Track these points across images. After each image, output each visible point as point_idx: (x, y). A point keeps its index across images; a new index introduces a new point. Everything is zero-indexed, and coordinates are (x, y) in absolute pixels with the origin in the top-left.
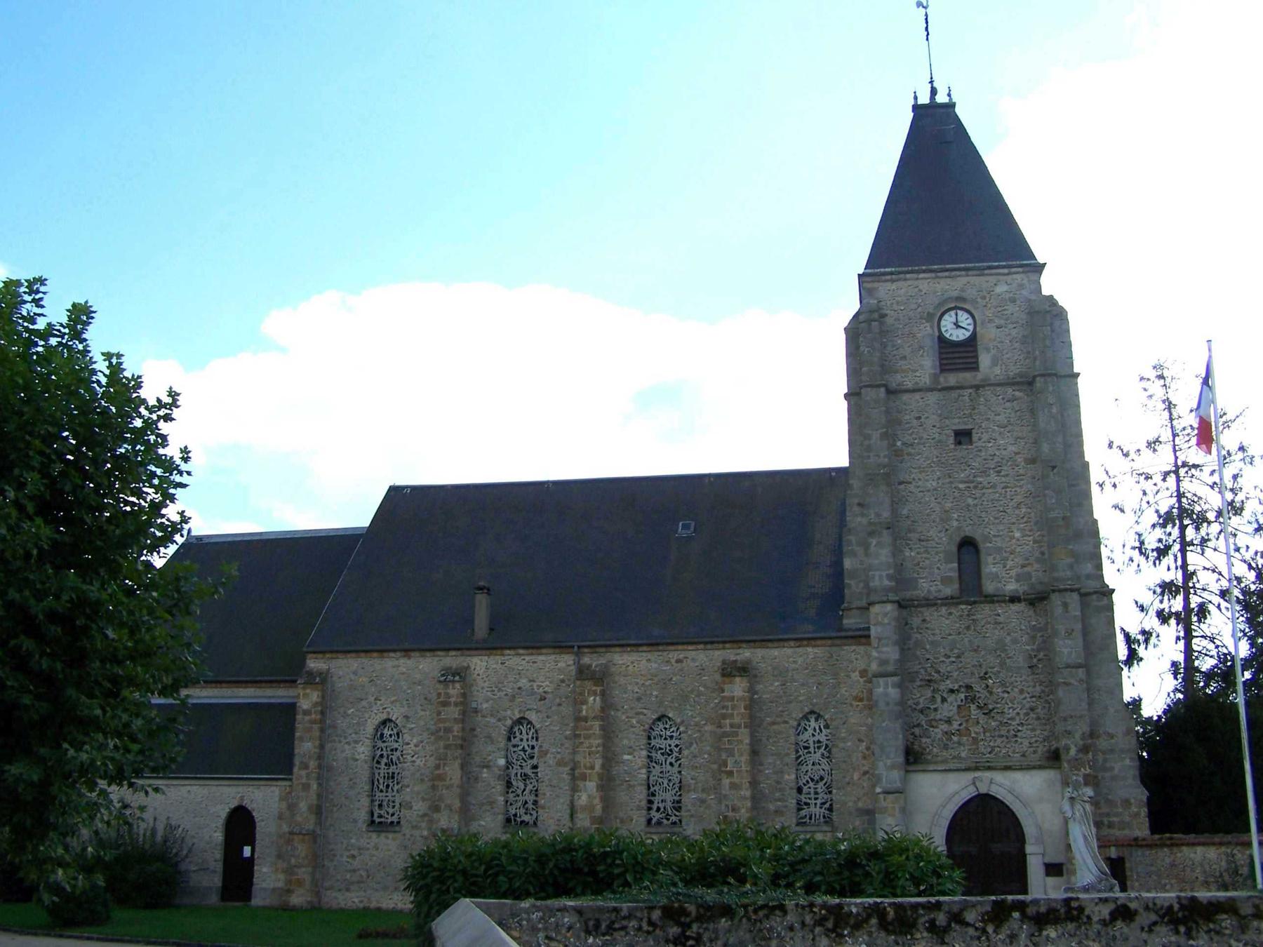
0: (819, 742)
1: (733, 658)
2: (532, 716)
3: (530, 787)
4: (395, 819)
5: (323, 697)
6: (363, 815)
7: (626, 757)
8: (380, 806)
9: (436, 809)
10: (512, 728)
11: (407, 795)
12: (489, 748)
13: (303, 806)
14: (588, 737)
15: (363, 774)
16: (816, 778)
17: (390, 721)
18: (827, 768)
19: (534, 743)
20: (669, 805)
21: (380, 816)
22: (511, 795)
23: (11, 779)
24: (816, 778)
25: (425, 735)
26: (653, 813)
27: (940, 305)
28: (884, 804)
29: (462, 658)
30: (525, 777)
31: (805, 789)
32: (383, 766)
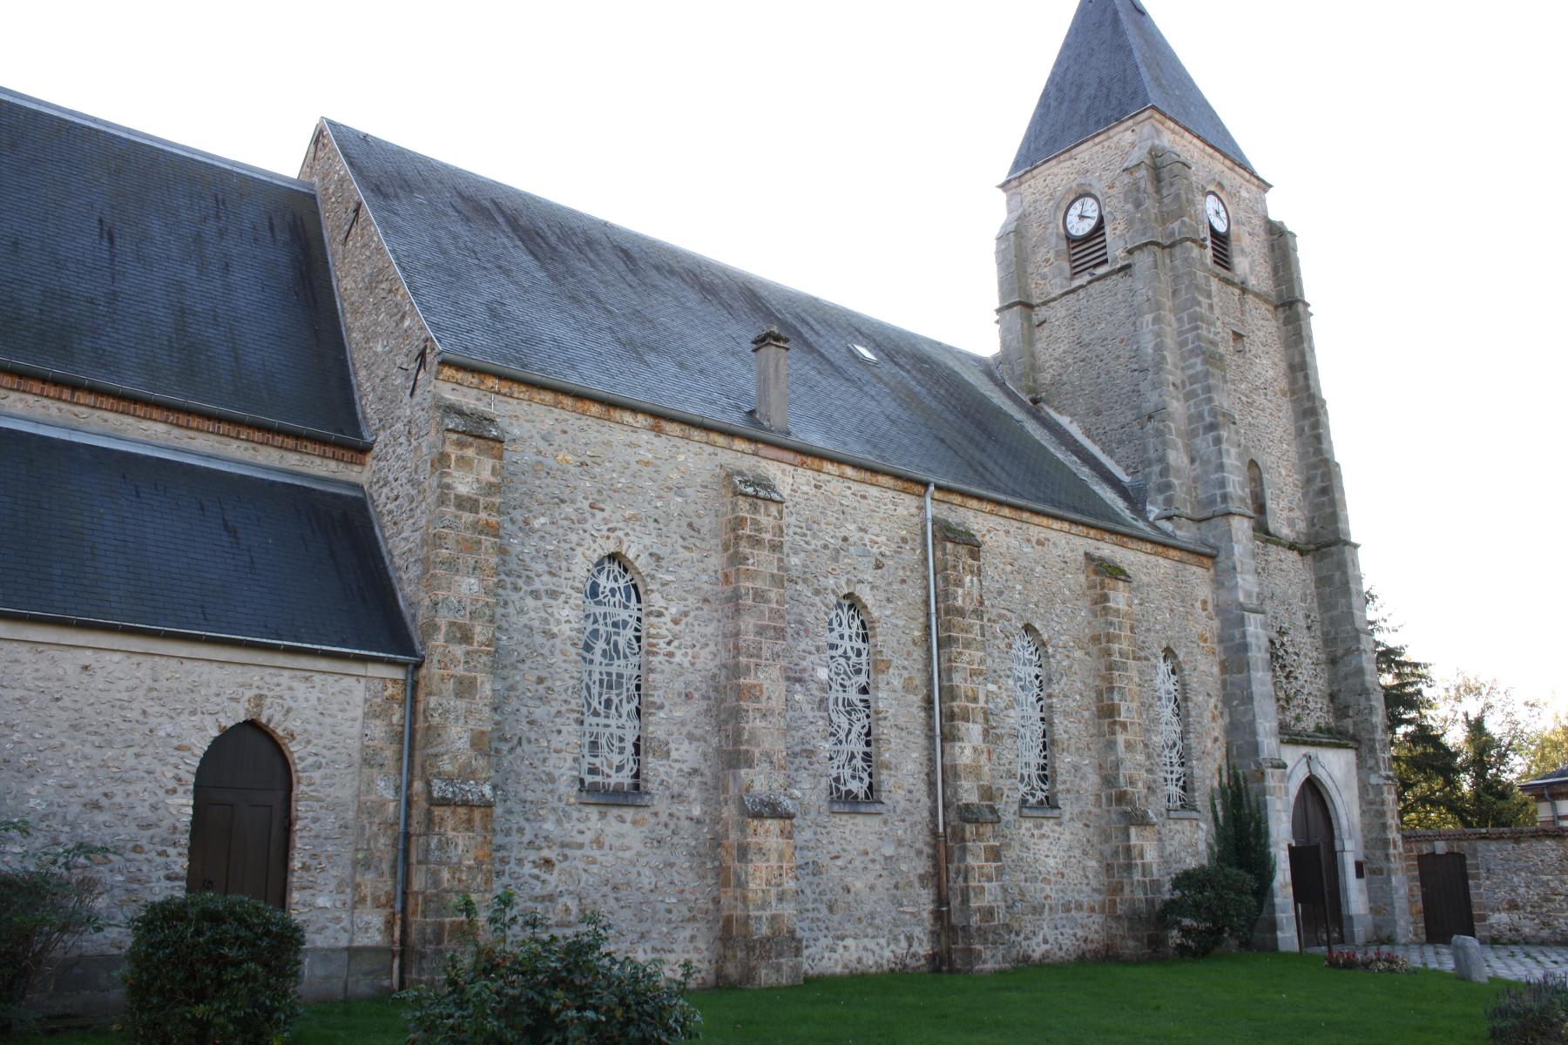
2: (866, 595)
3: (857, 728)
6: (564, 770)
12: (802, 646)
15: (565, 667)
19: (859, 644)
20: (1034, 772)
25: (692, 600)
27: (1058, 206)
32: (598, 657)
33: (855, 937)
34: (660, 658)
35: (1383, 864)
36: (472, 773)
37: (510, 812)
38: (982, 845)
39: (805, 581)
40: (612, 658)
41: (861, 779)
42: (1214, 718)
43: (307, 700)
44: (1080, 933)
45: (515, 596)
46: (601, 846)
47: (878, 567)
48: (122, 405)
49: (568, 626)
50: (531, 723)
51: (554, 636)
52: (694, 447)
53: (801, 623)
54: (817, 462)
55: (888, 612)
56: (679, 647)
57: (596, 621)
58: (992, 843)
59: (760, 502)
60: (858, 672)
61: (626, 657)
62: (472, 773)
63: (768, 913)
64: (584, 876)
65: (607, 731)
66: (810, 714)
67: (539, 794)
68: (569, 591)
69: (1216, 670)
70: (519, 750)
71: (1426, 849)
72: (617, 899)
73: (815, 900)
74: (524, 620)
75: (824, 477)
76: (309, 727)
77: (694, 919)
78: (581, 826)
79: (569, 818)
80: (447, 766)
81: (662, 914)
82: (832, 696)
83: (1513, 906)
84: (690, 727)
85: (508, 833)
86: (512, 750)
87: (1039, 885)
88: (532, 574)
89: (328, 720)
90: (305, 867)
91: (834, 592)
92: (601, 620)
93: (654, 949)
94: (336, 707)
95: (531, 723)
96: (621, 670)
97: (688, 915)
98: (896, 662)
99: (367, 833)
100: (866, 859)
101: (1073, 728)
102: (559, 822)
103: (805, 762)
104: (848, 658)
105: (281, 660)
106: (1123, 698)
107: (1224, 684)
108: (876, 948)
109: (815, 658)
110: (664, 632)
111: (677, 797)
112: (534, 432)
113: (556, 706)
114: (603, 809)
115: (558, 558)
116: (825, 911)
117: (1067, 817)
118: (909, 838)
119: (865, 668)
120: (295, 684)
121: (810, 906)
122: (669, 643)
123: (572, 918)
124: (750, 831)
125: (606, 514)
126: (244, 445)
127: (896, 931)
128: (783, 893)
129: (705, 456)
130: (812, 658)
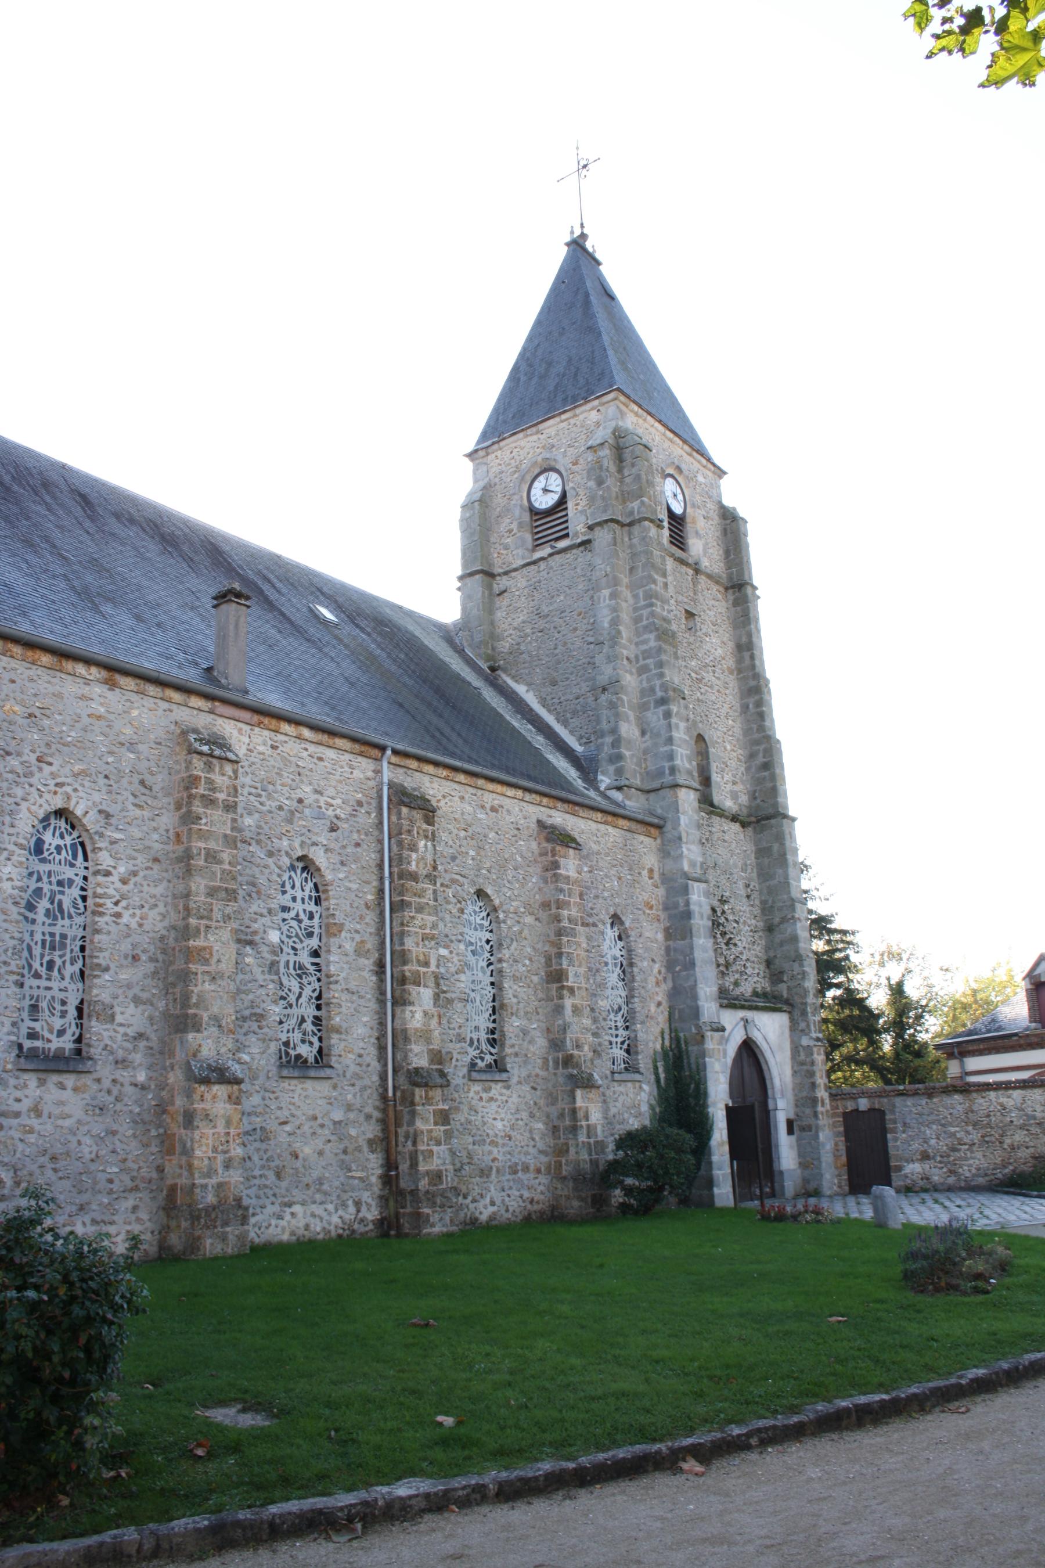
2: (320, 858)
3: (307, 991)
4: (66, 1043)
12: (254, 908)
14: (420, 909)
23: (588, 1166)
25: (141, 860)
29: (209, 718)
32: (40, 917)
33: (303, 1204)
34: (107, 918)
35: (812, 1121)
38: (431, 1108)
39: (259, 842)
40: (55, 918)
41: (311, 1043)
42: (657, 983)
44: (526, 1194)
49: (9, 884)
52: (149, 702)
53: (254, 885)
54: (274, 722)
55: (341, 876)
56: (126, 908)
57: (39, 879)
58: (441, 1107)
61: (70, 917)
63: (214, 1181)
64: (20, 1146)
65: (49, 994)
66: (260, 977)
69: (660, 936)
71: (850, 1106)
72: (55, 1170)
73: (263, 1167)
77: (136, 1189)
78: (19, 1094)
81: (103, 1185)
82: (283, 959)
83: (925, 1157)
84: (136, 990)
87: (487, 1148)
91: (287, 853)
92: (45, 878)
93: (94, 1222)
96: (65, 931)
97: (130, 1184)
98: (349, 925)
103: (254, 1026)
104: (300, 921)
107: (668, 949)
108: (324, 1214)
109: (266, 920)
110: (111, 891)
111: (121, 1063)
114: (42, 1076)
117: (514, 1080)
119: (317, 931)
122: (116, 904)
124: (196, 1097)
125: (53, 769)
127: (345, 1196)
128: (230, 1160)
129: (160, 712)
130: (263, 920)
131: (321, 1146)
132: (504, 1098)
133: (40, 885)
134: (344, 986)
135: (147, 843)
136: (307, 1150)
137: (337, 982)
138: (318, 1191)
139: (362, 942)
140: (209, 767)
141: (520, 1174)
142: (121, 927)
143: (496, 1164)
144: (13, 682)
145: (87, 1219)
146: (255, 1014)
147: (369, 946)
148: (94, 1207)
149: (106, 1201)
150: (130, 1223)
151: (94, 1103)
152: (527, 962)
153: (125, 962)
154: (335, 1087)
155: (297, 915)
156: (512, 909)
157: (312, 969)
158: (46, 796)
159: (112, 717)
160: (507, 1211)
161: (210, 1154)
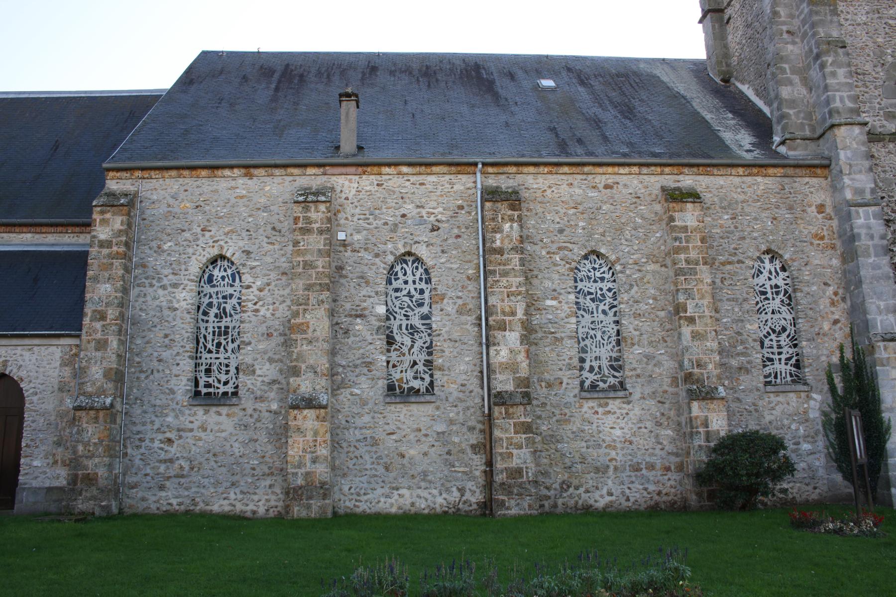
0: (777, 286)
1: (673, 185)
2: (422, 251)
4: (229, 388)
5: (129, 225)
6: (182, 386)
7: (549, 303)
8: (208, 371)
9: (295, 372)
10: (392, 267)
11: (246, 356)
12: (364, 293)
13: (96, 372)
14: (505, 274)
15: (183, 327)
16: (778, 329)
17: (223, 257)
18: (789, 317)
19: (423, 285)
20: (605, 363)
21: (208, 385)
22: (394, 354)
24: (778, 329)
25: (273, 275)
26: (586, 374)
28: (884, 355)
29: (325, 178)
30: (413, 330)
31: (767, 342)
33: (409, 488)
34: (249, 314)
36: (104, 391)
37: (145, 412)
38: (511, 421)
39: (366, 249)
40: (221, 318)
41: (423, 379)
42: (833, 304)
43: (30, 360)
44: (652, 488)
45: (151, 290)
46: (205, 430)
47: (434, 229)
48: (8, 229)
49: (185, 302)
50: (160, 361)
51: (176, 309)
52: (278, 180)
53: (362, 278)
54: (376, 169)
55: (443, 260)
56: (263, 306)
57: (211, 297)
58: (522, 419)
59: (311, 205)
60: (421, 305)
61: (231, 316)
62: (104, 391)
63: (303, 470)
64: (194, 448)
65: (217, 362)
66: (369, 338)
67: (164, 401)
68: (186, 282)
69: (835, 262)
70: (151, 377)
72: (216, 462)
73: (373, 463)
74: (157, 303)
75: (384, 177)
76: (31, 374)
77: (272, 474)
78: (192, 419)
79: (183, 414)
80: (89, 389)
81: (248, 471)
82: (395, 324)
84: (270, 354)
85: (144, 424)
86: (147, 377)
87: (603, 451)
88: (162, 276)
89: (42, 370)
90: (27, 446)
91: (391, 253)
92: (214, 296)
93: (242, 492)
94: (45, 362)
95: (160, 361)
96: (227, 324)
97: (267, 471)
98: (450, 293)
99: (60, 427)
100: (419, 434)
101: (646, 327)
102: (177, 417)
103: (365, 370)
104: (412, 297)
105: (15, 341)
106: (690, 296)
107: (844, 272)
108: (429, 497)
109: (375, 300)
110: (251, 297)
111: (259, 399)
112: (166, 195)
113: (176, 350)
114: (207, 408)
115: (179, 263)
116: (381, 470)
117: (637, 396)
118: (461, 417)
119: (427, 301)
120: (24, 353)
121: (368, 466)
122: (255, 304)
123: (185, 473)
124: (291, 417)
125: (212, 233)
126: (72, 235)
127: (448, 485)
128: (317, 457)
129: (287, 183)
130: (372, 300)
131: (426, 449)
132: (624, 411)
133: (211, 300)
134: (446, 337)
135: (277, 264)
136: (412, 452)
137: (439, 335)
138: (424, 480)
139: (464, 304)
140: (307, 209)
141: (644, 472)
142: (259, 318)
143: (614, 463)
144: (186, 191)
145: (238, 491)
146: (365, 362)
147: (471, 306)
148: (242, 484)
149: (250, 480)
150: (267, 495)
151: (241, 423)
152: (651, 301)
153: (262, 338)
154: (438, 408)
155: (409, 292)
156: (631, 261)
157: (423, 328)
158: (208, 249)
159: (251, 195)
160: (628, 500)
161: (301, 453)
